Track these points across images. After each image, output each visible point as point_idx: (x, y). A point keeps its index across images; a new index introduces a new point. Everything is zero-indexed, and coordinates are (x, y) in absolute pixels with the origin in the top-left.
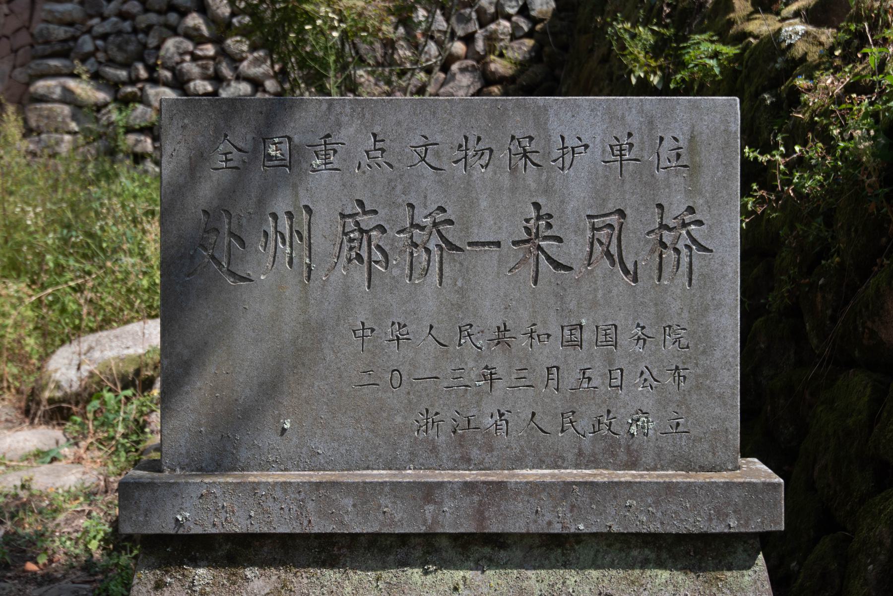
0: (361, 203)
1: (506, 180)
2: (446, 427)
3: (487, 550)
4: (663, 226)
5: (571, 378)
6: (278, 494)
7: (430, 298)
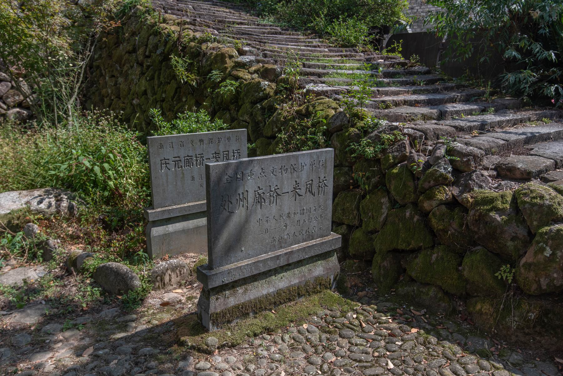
0: (259, 187)
1: (290, 176)
2: (277, 240)
3: (287, 267)
4: (320, 182)
5: (302, 222)
6: (246, 267)
7: (274, 208)
